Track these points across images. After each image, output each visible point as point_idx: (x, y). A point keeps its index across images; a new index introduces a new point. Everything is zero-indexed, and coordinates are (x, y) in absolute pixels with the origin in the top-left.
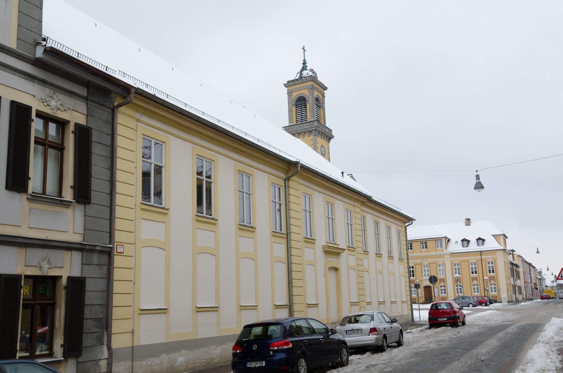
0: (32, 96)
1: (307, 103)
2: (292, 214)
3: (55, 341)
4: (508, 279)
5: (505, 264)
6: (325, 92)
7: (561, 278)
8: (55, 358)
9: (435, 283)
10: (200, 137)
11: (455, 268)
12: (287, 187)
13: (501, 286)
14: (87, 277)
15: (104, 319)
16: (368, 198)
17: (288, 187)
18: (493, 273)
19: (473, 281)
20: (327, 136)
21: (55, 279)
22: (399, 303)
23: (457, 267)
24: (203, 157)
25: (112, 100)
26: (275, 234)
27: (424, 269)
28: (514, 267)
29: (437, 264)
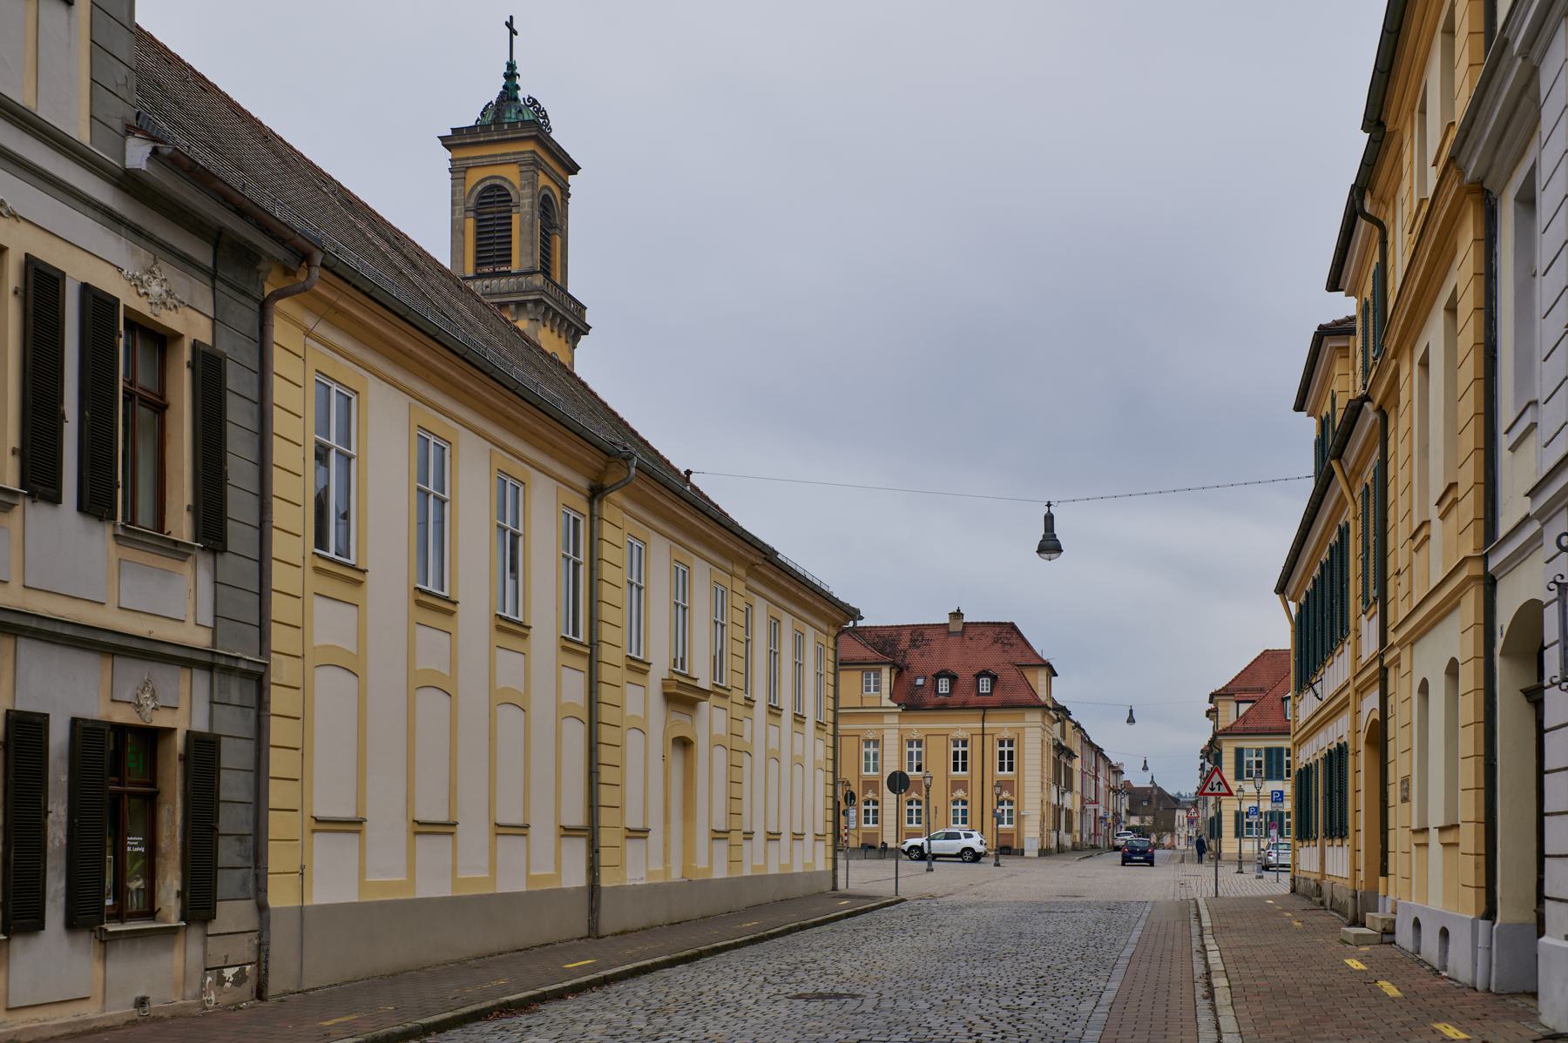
0: (115, 269)
1: (514, 210)
2: (607, 592)
3: (160, 881)
4: (1045, 791)
5: (1042, 749)
6: (571, 179)
7: (1210, 792)
8: (164, 921)
9: (903, 790)
10: (425, 379)
11: (911, 754)
12: (596, 518)
13: (1027, 807)
14: (224, 736)
15: (251, 838)
16: (766, 554)
17: (599, 519)
18: (962, 770)
19: (953, 791)
20: (570, 325)
21: (153, 737)
22: (809, 838)
23: (915, 749)
24: (429, 432)
25: (261, 276)
26: (567, 646)
27: (865, 750)
28: (1063, 759)
29: (861, 739)
